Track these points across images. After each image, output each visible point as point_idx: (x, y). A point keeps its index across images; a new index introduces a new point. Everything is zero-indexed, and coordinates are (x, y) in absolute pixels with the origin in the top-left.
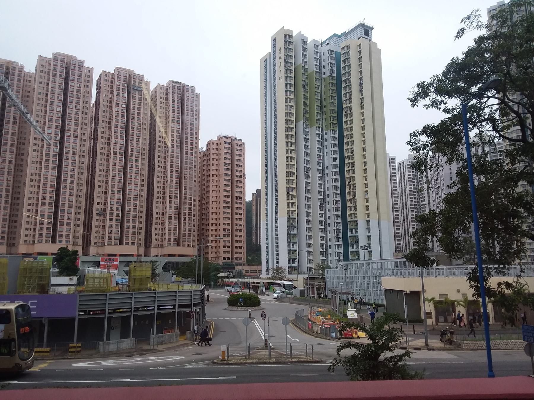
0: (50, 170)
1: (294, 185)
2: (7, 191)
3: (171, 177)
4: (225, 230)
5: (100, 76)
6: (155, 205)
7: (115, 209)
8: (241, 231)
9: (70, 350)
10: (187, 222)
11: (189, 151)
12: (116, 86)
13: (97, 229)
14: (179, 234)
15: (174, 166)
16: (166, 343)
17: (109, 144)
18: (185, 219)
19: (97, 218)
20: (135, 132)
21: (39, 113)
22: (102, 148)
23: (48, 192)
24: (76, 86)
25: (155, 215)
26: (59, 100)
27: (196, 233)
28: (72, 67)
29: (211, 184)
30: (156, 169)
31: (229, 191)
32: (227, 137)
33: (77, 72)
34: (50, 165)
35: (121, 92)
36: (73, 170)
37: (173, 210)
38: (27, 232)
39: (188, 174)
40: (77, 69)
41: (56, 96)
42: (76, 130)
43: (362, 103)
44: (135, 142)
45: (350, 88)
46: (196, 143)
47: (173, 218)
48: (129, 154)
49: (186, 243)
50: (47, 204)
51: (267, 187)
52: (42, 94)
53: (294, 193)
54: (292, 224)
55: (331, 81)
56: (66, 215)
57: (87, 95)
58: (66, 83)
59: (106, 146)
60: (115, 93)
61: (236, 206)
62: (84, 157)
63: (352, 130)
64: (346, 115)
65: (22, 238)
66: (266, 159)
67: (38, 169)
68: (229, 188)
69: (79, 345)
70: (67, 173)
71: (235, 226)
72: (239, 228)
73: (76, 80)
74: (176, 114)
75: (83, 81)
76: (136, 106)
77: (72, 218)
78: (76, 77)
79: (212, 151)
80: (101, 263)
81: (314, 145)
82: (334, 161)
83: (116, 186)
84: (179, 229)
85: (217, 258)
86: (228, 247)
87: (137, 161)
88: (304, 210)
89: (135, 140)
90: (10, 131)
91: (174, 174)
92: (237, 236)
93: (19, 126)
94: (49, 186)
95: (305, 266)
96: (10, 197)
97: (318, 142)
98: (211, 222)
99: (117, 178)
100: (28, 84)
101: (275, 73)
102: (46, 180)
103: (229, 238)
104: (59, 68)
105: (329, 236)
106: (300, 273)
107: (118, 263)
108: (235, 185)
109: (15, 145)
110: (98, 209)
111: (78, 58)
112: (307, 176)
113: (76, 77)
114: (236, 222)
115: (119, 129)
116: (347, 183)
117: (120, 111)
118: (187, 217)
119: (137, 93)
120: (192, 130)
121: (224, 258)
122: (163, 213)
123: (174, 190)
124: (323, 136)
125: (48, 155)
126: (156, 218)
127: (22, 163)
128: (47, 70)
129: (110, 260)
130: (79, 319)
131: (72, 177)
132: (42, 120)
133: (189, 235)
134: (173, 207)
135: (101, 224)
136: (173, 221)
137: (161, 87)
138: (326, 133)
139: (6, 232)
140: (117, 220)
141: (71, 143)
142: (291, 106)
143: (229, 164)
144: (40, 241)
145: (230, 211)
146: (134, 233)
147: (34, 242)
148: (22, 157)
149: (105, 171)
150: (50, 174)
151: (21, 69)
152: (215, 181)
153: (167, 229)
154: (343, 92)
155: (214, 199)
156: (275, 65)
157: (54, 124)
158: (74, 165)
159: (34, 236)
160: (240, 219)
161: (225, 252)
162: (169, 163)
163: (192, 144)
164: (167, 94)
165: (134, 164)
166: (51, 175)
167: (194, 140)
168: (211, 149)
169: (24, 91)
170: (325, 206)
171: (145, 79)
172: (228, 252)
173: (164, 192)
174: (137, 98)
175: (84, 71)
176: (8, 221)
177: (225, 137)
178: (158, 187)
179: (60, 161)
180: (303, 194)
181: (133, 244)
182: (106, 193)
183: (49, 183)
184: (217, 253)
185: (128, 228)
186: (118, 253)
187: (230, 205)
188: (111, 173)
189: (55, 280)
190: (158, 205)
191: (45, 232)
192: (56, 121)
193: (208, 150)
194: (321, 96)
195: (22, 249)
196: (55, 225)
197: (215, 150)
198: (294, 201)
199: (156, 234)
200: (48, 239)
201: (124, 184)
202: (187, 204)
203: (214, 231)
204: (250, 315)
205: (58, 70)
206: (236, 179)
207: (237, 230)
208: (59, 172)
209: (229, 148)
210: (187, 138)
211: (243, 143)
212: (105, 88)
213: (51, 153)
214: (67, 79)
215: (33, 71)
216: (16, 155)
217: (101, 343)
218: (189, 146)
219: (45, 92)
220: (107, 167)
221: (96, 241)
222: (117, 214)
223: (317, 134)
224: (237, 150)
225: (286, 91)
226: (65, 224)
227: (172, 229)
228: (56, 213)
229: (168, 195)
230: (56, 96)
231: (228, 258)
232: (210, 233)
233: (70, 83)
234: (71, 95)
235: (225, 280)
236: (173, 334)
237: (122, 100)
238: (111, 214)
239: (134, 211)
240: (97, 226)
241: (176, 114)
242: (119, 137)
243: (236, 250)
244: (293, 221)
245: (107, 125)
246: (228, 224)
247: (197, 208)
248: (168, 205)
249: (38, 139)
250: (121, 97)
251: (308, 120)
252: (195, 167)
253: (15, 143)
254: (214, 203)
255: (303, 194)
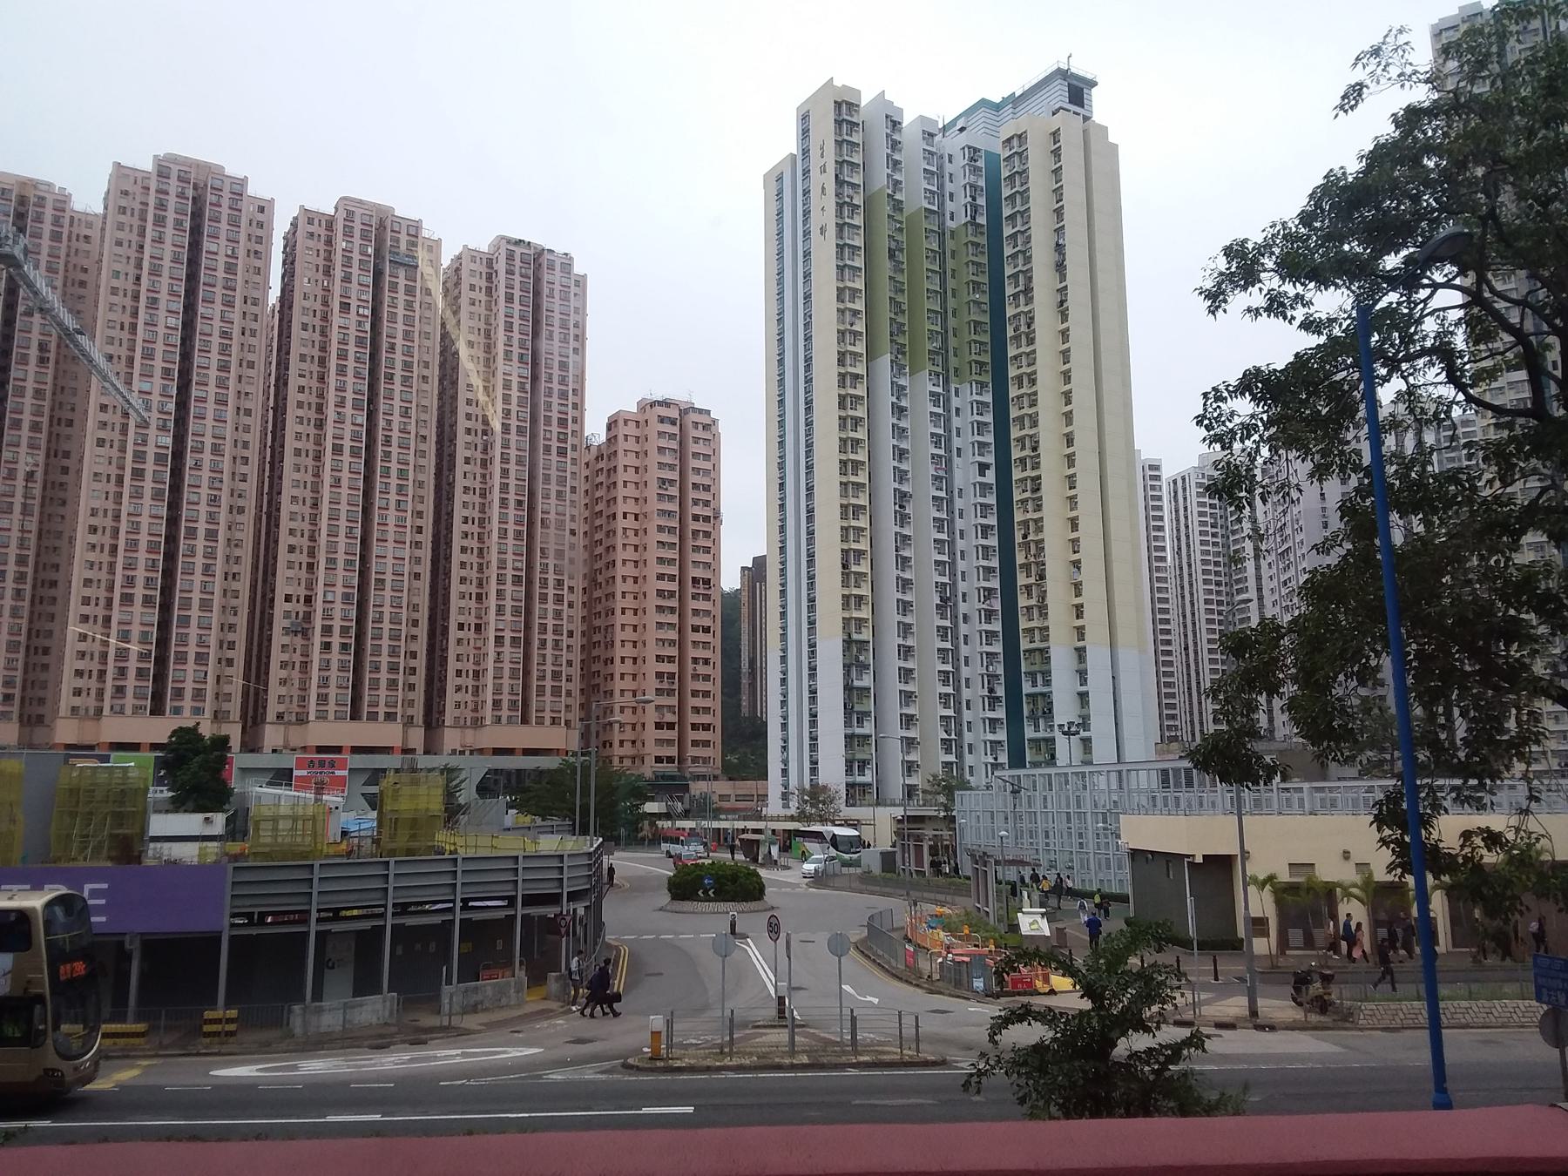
0: (147, 500)
1: (864, 545)
2: (21, 561)
3: (503, 519)
4: (660, 675)
5: (294, 224)
6: (455, 602)
7: (337, 614)
8: (707, 678)
9: (207, 1028)
10: (549, 651)
11: (555, 444)
12: (339, 253)
13: (283, 674)
14: (526, 687)
15: (512, 489)
16: (486, 1010)
17: (320, 425)
18: (543, 643)
19: (286, 640)
20: (397, 387)
21: (116, 333)
22: (298, 436)
23: (141, 564)
24: (222, 252)
25: (454, 634)
26: (172, 293)
27: (576, 686)
28: (210, 198)
29: (619, 541)
30: (459, 497)
31: (671, 561)
32: (666, 404)
33: (225, 211)
34: (148, 485)
35: (355, 271)
36: (214, 501)
37: (508, 617)
38: (80, 683)
39: (553, 511)
40: (225, 202)
41: (165, 281)
42: (222, 384)
43: (1062, 303)
44: (396, 419)
45: (1028, 260)
46: (575, 421)
47: (507, 641)
48: (380, 454)
49: (548, 715)
50: (138, 600)
51: (783, 550)
52: (122, 277)
53: (864, 567)
54: (857, 658)
55: (971, 238)
56: (193, 631)
57: (257, 279)
58: (195, 245)
59: (312, 431)
60: (338, 273)
61: (693, 604)
62: (246, 460)
63: (1033, 382)
64: (1017, 338)
65: (66, 700)
66: (781, 466)
67: (111, 496)
68: (673, 554)
69: (233, 1013)
70: (196, 507)
71: (690, 666)
72: (701, 669)
73: (223, 236)
74: (516, 336)
75: (243, 237)
76: (401, 311)
77: (213, 641)
78: (224, 226)
79: (621, 445)
80: (295, 773)
81: (922, 425)
82: (982, 474)
83: (341, 548)
84: (527, 673)
85: (638, 759)
86: (671, 726)
87: (402, 474)
88: (892, 617)
89: (397, 412)
90: (30, 386)
91: (512, 512)
92: (695, 693)
93: (56, 370)
94: (143, 546)
95: (896, 782)
96: (29, 579)
97: (932, 418)
98: (619, 652)
99: (343, 523)
100: (84, 246)
101: (806, 213)
102: (135, 528)
103: (674, 701)
104: (172, 201)
105: (966, 694)
106: (880, 802)
107: (345, 773)
108: (690, 543)
109: (45, 427)
110: (287, 615)
111: (229, 171)
112: (903, 519)
113: (224, 226)
114: (692, 653)
115: (350, 379)
116: (1018, 539)
117: (353, 327)
118: (550, 637)
119: (402, 273)
120: (563, 381)
121: (659, 760)
122: (478, 628)
123: (510, 557)
124: (947, 401)
125: (139, 457)
126: (459, 641)
127: (64, 478)
128: (137, 207)
129: (322, 763)
130: (232, 938)
131: (212, 519)
132: (124, 352)
133: (556, 691)
134: (508, 610)
135: (297, 658)
136: (507, 648)
137: (474, 255)
138: (957, 390)
139: (19, 681)
140: (344, 646)
141: (209, 422)
142: (855, 313)
143: (672, 482)
144: (117, 708)
145: (674, 619)
146: (392, 684)
147: (99, 711)
148: (65, 462)
149: (309, 502)
150: (146, 512)
151: (62, 202)
152: (630, 533)
153: (490, 673)
154: (1009, 271)
155: (629, 586)
156: (806, 192)
157: (158, 364)
158: (217, 485)
159: (100, 693)
160: (706, 644)
161: (660, 742)
162: (497, 480)
163: (562, 423)
164: (489, 278)
165: (394, 481)
166: (150, 513)
167: (571, 413)
168: (621, 438)
169: (70, 267)
170: (955, 604)
171: (425, 233)
172: (669, 742)
173: (481, 565)
174: (401, 289)
175: (248, 210)
176: (22, 650)
177: (660, 403)
178: (464, 550)
179: (177, 473)
180: (890, 572)
181: (390, 717)
182: (311, 566)
183: (144, 539)
184: (639, 744)
185: (377, 669)
186: (347, 742)
187: (674, 603)
188: (325, 507)
189: (161, 824)
190: (463, 603)
191: (131, 682)
192: (164, 355)
193: (611, 440)
194: (943, 283)
195: (66, 731)
196: (161, 661)
197: (632, 440)
198: (865, 590)
199: (458, 689)
200: (142, 703)
201: (365, 541)
202: (551, 599)
203: (628, 678)
204: (733, 925)
205: (171, 205)
206: (693, 526)
207: (696, 677)
208: (174, 506)
209: (672, 436)
210: (549, 406)
211: (714, 421)
212: (307, 258)
213: (151, 451)
214: (196, 231)
215: (98, 208)
216: (48, 456)
217: (297, 1008)
218: (555, 429)
219: (132, 271)
220: (315, 490)
221: (281, 708)
222: (344, 631)
223: (932, 394)
224: (696, 440)
225: (841, 269)
226: (191, 657)
227: (507, 673)
228: (164, 625)
229: (493, 572)
230: (165, 281)
231: (670, 760)
232: (618, 685)
233: (207, 245)
234: (208, 280)
235: (660, 823)
236: (508, 983)
237: (359, 294)
238: (327, 630)
239: (395, 620)
240: (284, 665)
241: (516, 336)
242: (349, 403)
243: (692, 735)
244: (859, 651)
245: (315, 368)
246: (670, 659)
247: (579, 612)
248: (492, 602)
249: (110, 410)
250: (354, 286)
251: (904, 354)
252: (573, 490)
253: (45, 420)
254: (630, 597)
255: (890, 572)
